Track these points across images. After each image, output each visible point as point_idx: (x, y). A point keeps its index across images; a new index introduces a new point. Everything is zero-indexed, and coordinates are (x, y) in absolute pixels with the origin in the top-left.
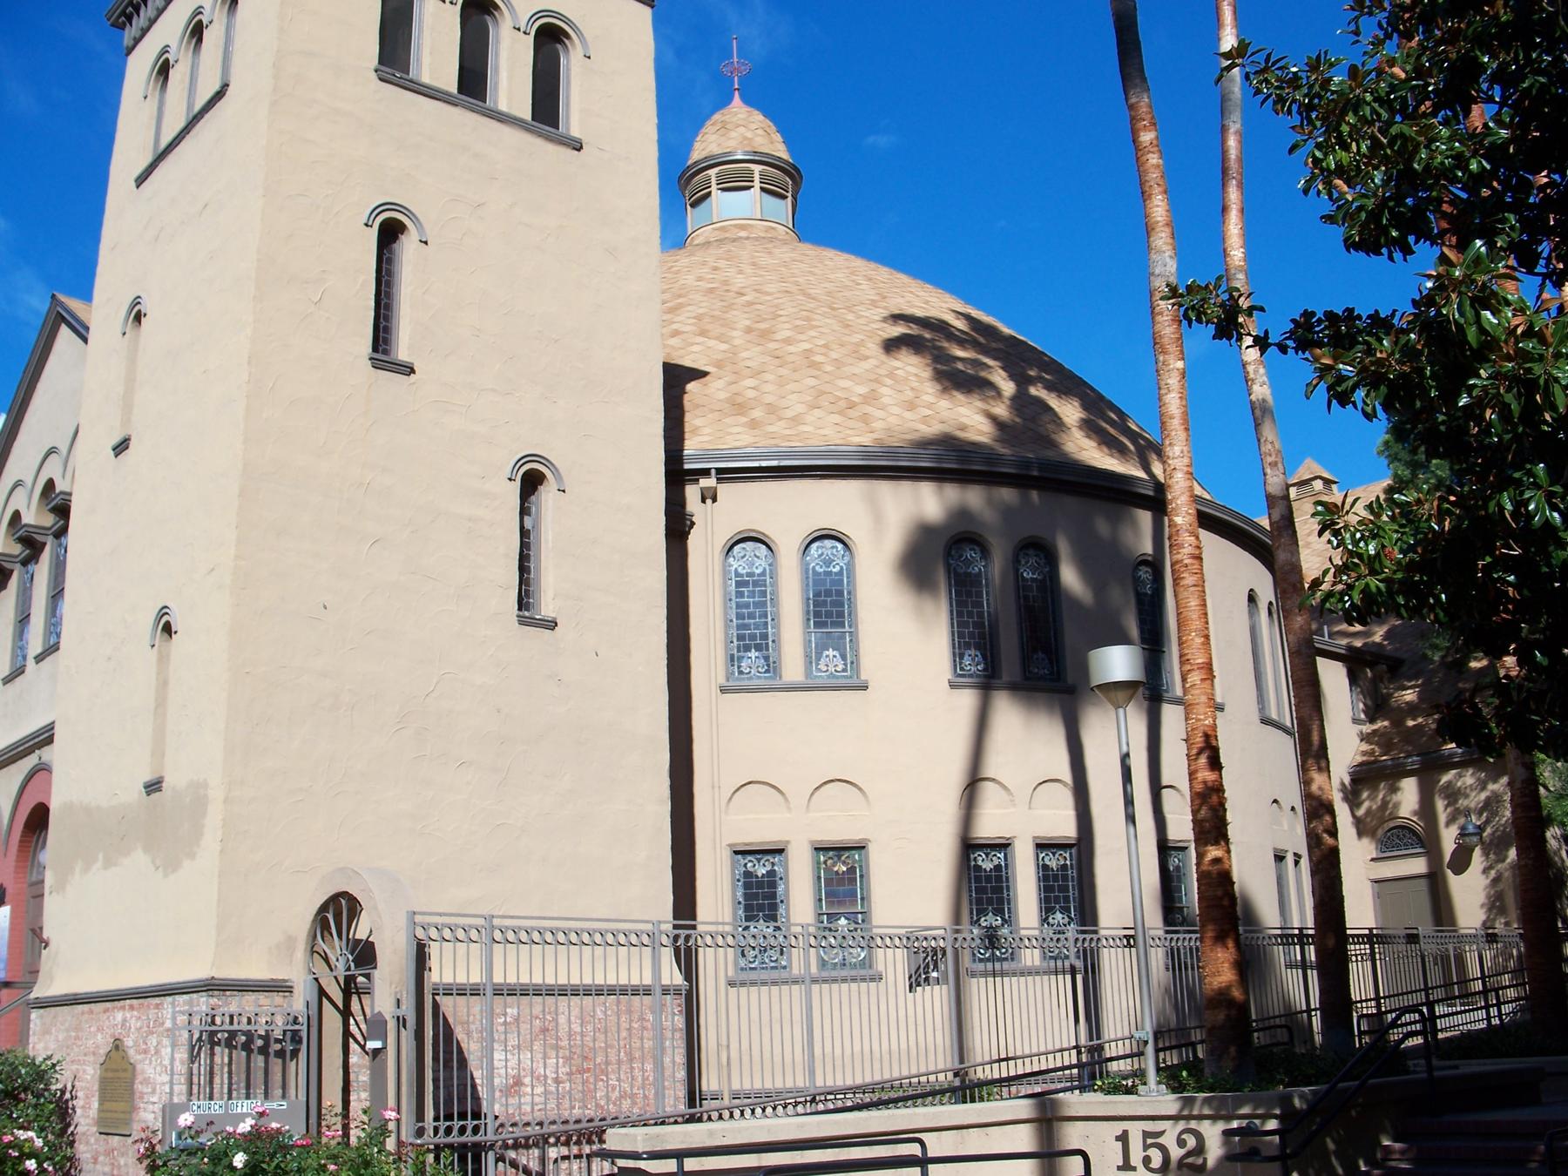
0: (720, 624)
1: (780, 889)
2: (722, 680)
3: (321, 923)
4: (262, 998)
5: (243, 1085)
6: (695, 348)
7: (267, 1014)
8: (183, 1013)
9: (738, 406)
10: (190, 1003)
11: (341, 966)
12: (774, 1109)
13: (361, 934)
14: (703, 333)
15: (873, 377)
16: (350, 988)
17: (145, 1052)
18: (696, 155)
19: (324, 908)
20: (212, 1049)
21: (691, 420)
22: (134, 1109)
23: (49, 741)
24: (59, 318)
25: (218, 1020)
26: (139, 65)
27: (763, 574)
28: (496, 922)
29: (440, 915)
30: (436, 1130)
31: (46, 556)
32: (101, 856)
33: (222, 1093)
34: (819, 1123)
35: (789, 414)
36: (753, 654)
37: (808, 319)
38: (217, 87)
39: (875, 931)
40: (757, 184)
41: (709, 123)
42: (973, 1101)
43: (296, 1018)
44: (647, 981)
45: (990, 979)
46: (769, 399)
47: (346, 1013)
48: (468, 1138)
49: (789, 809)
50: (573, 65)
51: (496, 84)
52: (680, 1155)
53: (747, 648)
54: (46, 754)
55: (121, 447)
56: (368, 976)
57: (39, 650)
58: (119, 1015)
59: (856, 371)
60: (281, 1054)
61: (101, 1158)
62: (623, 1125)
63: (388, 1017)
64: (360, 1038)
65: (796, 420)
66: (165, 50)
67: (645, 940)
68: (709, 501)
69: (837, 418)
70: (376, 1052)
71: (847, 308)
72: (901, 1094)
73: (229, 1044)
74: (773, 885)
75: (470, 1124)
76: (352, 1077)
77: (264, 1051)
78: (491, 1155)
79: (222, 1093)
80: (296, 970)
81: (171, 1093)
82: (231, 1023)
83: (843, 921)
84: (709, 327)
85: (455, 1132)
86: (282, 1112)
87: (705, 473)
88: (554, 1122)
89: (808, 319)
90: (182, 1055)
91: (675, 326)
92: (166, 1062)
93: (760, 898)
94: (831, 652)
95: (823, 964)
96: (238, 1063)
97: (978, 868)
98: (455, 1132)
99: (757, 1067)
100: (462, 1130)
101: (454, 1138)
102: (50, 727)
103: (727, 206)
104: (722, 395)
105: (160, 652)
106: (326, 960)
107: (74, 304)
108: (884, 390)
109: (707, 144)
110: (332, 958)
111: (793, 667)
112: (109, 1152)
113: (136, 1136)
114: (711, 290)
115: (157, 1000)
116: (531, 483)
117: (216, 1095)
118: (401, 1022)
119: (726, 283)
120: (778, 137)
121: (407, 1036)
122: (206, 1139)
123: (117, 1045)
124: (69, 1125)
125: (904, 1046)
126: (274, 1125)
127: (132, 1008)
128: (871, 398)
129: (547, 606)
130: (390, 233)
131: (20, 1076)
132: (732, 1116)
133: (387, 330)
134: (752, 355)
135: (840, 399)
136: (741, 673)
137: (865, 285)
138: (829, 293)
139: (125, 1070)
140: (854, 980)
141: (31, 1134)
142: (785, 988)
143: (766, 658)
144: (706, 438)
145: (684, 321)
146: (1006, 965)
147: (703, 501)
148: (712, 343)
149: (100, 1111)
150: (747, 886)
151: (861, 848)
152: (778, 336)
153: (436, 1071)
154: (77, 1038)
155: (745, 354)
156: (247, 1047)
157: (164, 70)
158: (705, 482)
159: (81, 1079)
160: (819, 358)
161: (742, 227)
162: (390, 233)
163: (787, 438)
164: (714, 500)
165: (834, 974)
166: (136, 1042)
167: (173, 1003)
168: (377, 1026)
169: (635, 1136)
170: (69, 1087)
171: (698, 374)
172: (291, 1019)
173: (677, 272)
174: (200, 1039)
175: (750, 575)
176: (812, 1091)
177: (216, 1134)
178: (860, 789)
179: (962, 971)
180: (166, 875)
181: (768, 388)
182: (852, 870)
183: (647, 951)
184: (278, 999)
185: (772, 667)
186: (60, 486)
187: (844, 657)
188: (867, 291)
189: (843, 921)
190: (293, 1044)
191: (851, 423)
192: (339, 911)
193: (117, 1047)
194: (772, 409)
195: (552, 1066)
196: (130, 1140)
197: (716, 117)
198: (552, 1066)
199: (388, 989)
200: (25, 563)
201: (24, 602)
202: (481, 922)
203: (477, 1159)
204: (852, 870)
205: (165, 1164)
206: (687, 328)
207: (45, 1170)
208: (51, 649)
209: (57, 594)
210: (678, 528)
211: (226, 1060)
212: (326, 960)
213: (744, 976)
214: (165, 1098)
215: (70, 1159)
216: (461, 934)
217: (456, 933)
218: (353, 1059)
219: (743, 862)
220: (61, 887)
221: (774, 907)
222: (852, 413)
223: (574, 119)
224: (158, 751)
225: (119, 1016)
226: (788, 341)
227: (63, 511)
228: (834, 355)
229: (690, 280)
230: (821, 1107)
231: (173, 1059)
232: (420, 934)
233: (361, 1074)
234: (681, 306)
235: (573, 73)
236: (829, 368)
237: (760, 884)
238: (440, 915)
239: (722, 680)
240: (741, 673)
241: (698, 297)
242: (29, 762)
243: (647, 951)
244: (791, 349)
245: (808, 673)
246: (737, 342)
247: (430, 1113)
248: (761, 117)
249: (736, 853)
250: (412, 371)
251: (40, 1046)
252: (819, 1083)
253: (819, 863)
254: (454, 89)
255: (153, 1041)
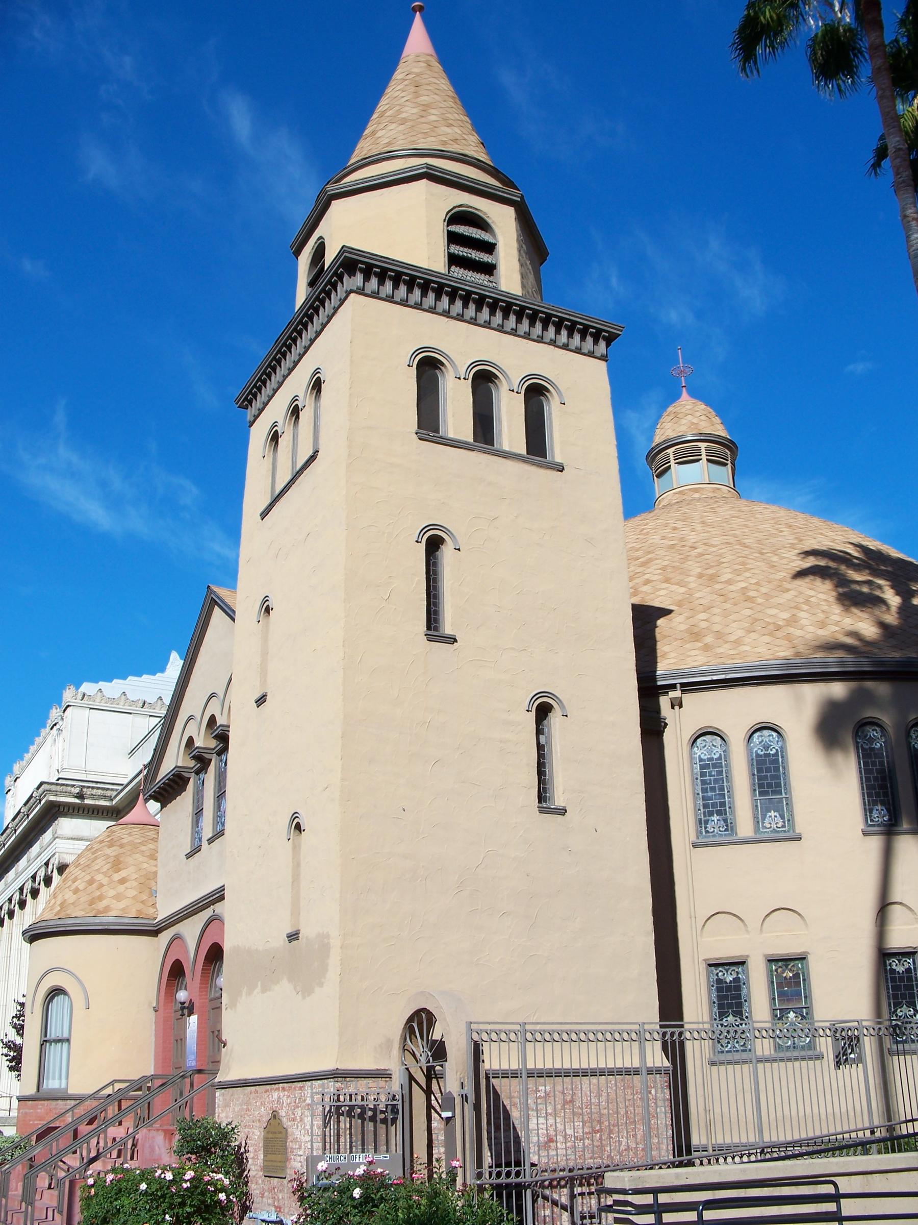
0: (690, 797)
1: (744, 992)
2: (693, 838)
3: (409, 1029)
4: (371, 1082)
5: (359, 1143)
6: (662, 592)
7: (375, 1094)
8: (317, 1093)
9: (695, 635)
10: (323, 1086)
11: (423, 1059)
12: (733, 1158)
13: (436, 1036)
14: (667, 580)
15: (793, 605)
16: (431, 1074)
17: (294, 1120)
18: (658, 439)
19: (411, 1019)
20: (338, 1118)
21: (662, 647)
22: (288, 1159)
23: (222, 898)
24: (212, 602)
25: (342, 1098)
26: (258, 434)
27: (720, 758)
28: (528, 1027)
29: (489, 1023)
30: (490, 1174)
31: (212, 768)
32: (259, 983)
33: (346, 1149)
34: (757, 1168)
35: (733, 638)
36: (715, 818)
37: (744, 564)
38: (310, 453)
39: (817, 1024)
40: (704, 457)
41: (665, 414)
42: (893, 1151)
43: (394, 1096)
44: (636, 1064)
45: (902, 1058)
46: (717, 628)
47: (428, 1092)
48: (512, 1180)
49: (747, 931)
50: (554, 412)
51: (500, 431)
52: (655, 1191)
53: (711, 814)
54: (218, 908)
55: (261, 700)
56: (442, 1066)
57: (211, 835)
58: (275, 1094)
59: (780, 601)
60: (385, 1121)
61: (266, 1194)
62: (622, 1170)
63: (455, 1095)
64: (438, 1109)
65: (738, 642)
66: (275, 425)
67: (634, 1036)
68: (677, 708)
69: (767, 639)
70: (448, 1119)
71: (774, 552)
72: (823, 1147)
73: (350, 1114)
74: (738, 988)
75: (514, 1170)
76: (434, 1136)
77: (373, 1119)
78: (529, 1192)
79: (346, 1149)
80: (393, 1063)
81: (312, 1149)
82: (351, 1100)
83: (792, 1015)
84: (670, 576)
85: (503, 1175)
86: (386, 1162)
87: (673, 687)
88: (563, 1170)
89: (744, 564)
90: (318, 1122)
91: (646, 577)
92: (308, 1127)
93: (729, 999)
94: (773, 814)
95: (778, 1047)
96: (356, 1128)
97: (893, 971)
98: (503, 1175)
99: (735, 1127)
100: (508, 1174)
101: (503, 1180)
102: (222, 889)
103: (683, 475)
104: (683, 627)
105: (293, 843)
106: (414, 1055)
107: (222, 592)
108: (802, 614)
109: (666, 430)
110: (418, 1055)
111: (745, 825)
112: (271, 1190)
113: (288, 1178)
114: (672, 546)
115: (300, 1084)
116: (543, 712)
117: (342, 1150)
118: (465, 1098)
119: (682, 539)
120: (717, 420)
121: (469, 1107)
122: (335, 1180)
123: (275, 1115)
124: (244, 1170)
125: (844, 1109)
126: (379, 1170)
127: (283, 1089)
128: (793, 621)
129: (559, 799)
130: (434, 545)
131: (212, 1136)
132: (701, 1164)
133: (436, 613)
134: (703, 595)
135: (769, 623)
136: (707, 832)
137: (786, 532)
138: (759, 542)
139: (281, 1133)
140: (803, 1059)
141: (220, 1176)
142: (738, 1067)
143: (725, 821)
144: (672, 661)
145: (653, 572)
146: (907, 1046)
147: (673, 707)
148: (674, 587)
149: (264, 1160)
150: (719, 990)
151: (802, 958)
152: (723, 579)
153: (489, 1132)
154: (248, 1110)
155: (698, 595)
156: (361, 1116)
157: (275, 438)
158: (673, 694)
159: (251, 1139)
160: (752, 594)
161: (696, 491)
162: (434, 545)
163: (732, 657)
164: (681, 706)
165: (789, 1054)
166: (287, 1113)
167: (311, 1086)
168: (448, 1102)
169: (624, 1177)
170: (243, 1144)
171: (665, 612)
172: (391, 1097)
173: (647, 534)
174: (330, 1111)
175: (711, 759)
176: (761, 1145)
177: (341, 1176)
178: (799, 914)
179: (886, 1051)
180: (304, 998)
181: (717, 619)
182: (797, 976)
183: (636, 1045)
184: (381, 1082)
185: (730, 827)
186: (220, 721)
187: (782, 817)
188: (788, 537)
189: (792, 1015)
190: (393, 1114)
191: (778, 642)
192: (420, 1021)
193: (275, 1117)
194: (719, 635)
195: (577, 1127)
196: (285, 1181)
197: (670, 409)
198: (577, 1127)
199: (455, 1076)
200: (197, 773)
201: (198, 802)
202: (517, 1027)
203: (519, 1197)
204: (797, 976)
205: (310, 1196)
206: (655, 578)
207: (231, 1201)
208: (219, 834)
209: (220, 795)
210: (652, 729)
211: (348, 1126)
212: (414, 1055)
213: (722, 1057)
214: (308, 1152)
215: (246, 1194)
216: (503, 1036)
217: (501, 1036)
218: (434, 1125)
219: (715, 972)
220: (233, 1004)
221: (740, 1005)
222: (779, 634)
223: (557, 449)
224: (296, 911)
225: (275, 1095)
226: (729, 582)
227: (223, 738)
228: (764, 590)
229: (656, 539)
230: (768, 1156)
231: (312, 1125)
232: (476, 1037)
233: (439, 1137)
234: (650, 561)
235: (554, 416)
236: (760, 601)
237: (729, 989)
238: (489, 1023)
239: (693, 838)
240: (707, 832)
241: (661, 552)
242: (206, 914)
243: (636, 1045)
244: (732, 588)
245: (757, 829)
246: (692, 585)
247: (488, 1159)
248: (703, 406)
249: (710, 965)
250: (455, 641)
251: (223, 1115)
252: (767, 1139)
253: (771, 971)
254: (470, 439)
255: (299, 1112)
